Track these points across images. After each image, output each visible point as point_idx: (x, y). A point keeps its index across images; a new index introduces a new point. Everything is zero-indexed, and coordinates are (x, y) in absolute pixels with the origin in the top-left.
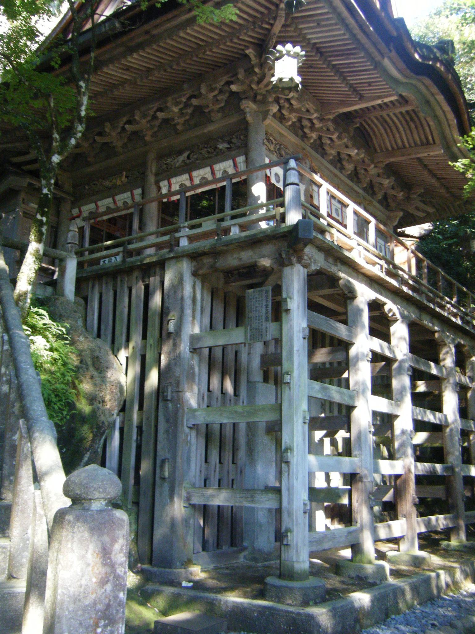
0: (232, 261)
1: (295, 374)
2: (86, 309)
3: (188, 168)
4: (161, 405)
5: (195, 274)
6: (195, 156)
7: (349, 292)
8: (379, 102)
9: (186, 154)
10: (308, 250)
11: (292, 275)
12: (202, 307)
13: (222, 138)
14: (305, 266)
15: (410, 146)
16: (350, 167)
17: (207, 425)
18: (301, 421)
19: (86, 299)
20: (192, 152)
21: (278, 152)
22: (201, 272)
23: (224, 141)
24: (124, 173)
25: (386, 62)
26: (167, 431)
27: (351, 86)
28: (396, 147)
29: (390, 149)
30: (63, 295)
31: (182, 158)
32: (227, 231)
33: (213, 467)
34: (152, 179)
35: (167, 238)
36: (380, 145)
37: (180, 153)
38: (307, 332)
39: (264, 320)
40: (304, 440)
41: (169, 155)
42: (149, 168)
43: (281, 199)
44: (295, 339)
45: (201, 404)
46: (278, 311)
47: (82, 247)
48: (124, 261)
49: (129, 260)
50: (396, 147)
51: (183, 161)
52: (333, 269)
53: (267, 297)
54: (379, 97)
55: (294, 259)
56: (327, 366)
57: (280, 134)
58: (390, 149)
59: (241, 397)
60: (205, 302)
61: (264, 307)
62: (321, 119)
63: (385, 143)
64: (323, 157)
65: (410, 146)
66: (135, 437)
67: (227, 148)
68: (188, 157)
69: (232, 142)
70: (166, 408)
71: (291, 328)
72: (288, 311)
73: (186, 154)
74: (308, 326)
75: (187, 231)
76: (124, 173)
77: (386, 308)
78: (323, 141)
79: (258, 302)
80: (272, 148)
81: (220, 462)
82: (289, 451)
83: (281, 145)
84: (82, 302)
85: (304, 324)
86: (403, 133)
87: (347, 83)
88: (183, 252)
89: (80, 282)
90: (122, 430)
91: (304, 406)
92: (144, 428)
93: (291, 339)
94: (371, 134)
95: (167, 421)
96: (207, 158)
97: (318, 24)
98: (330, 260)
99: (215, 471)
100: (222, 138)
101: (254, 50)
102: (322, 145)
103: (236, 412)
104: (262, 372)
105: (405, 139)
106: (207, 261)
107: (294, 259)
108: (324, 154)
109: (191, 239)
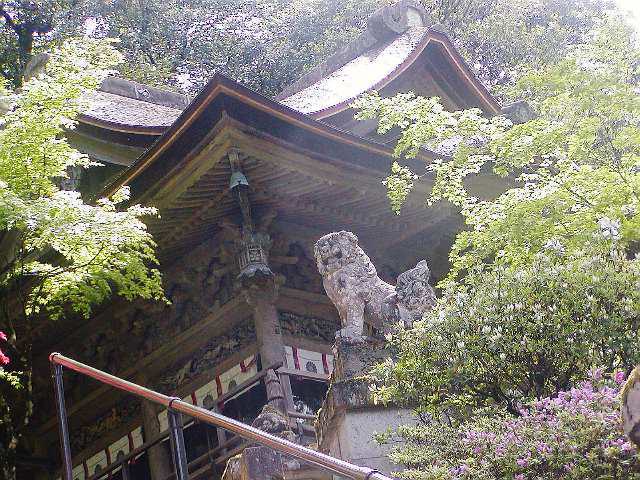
9: (188, 366)
31: (183, 372)
37: (180, 365)
51: (186, 376)
68: (192, 370)
73: (188, 366)
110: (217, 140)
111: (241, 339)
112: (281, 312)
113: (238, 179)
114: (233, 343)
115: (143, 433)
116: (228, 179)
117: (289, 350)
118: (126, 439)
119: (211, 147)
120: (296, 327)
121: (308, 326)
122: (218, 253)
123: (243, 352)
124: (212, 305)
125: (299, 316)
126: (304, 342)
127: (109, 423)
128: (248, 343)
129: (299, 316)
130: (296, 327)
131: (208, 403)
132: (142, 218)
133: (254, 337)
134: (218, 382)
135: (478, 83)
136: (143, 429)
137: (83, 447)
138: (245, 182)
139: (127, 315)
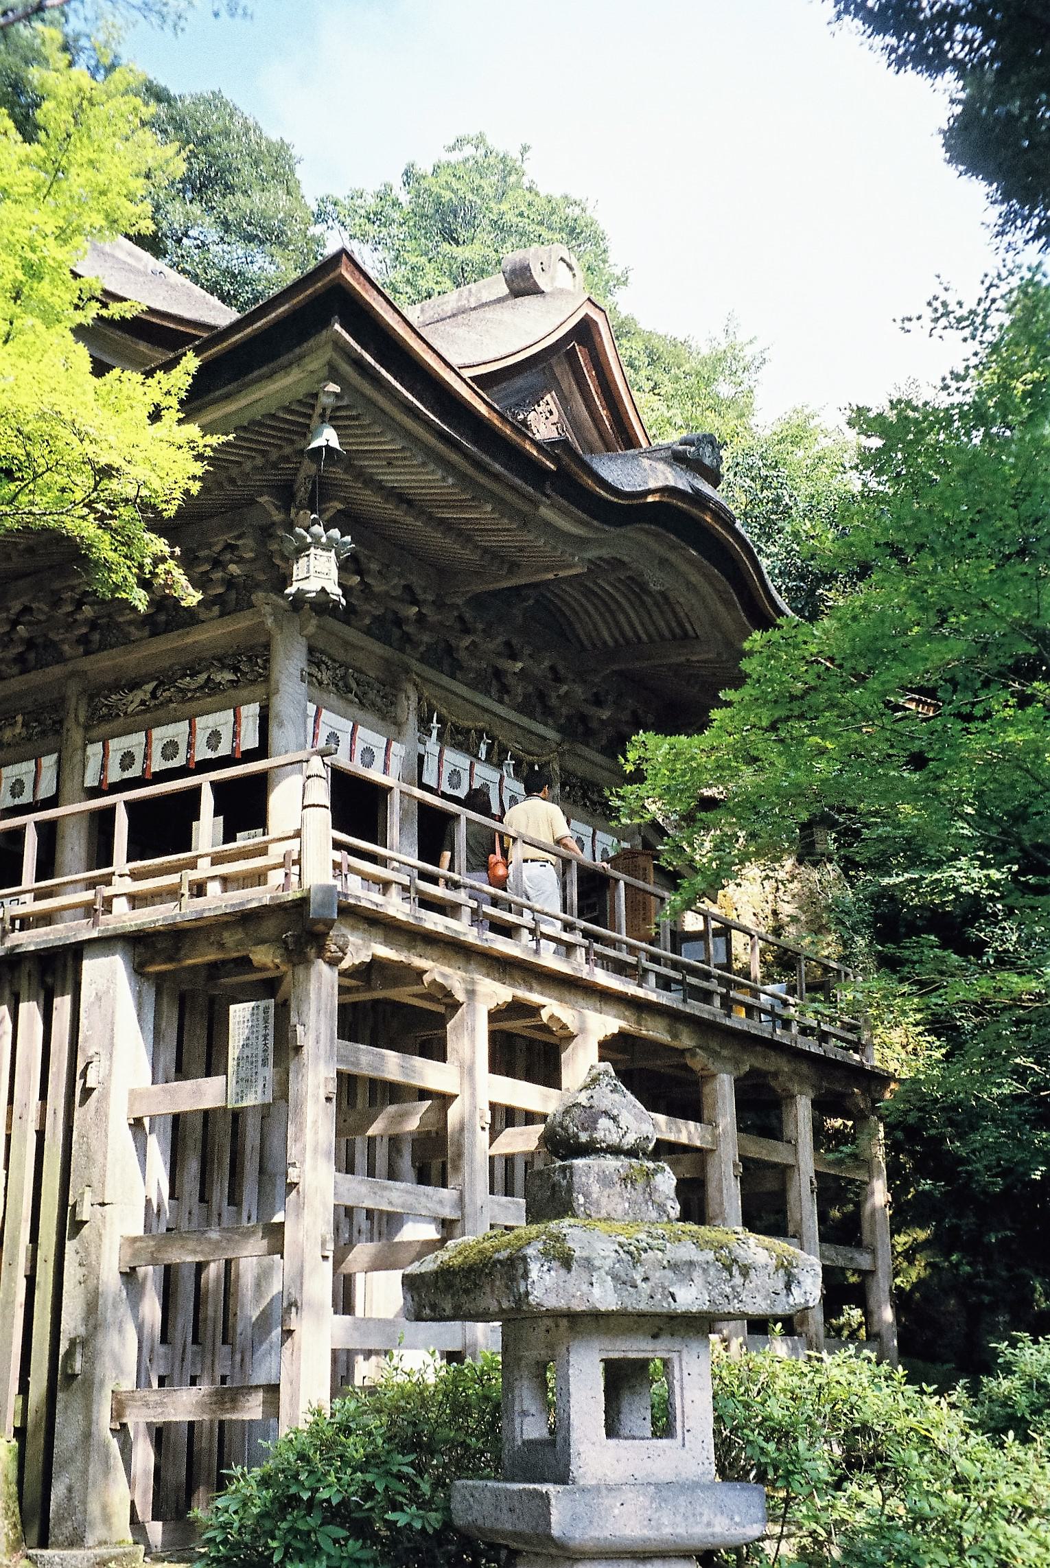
3: (149, 718)
6: (167, 694)
7: (445, 996)
8: (551, 576)
9: (149, 687)
11: (308, 980)
13: (222, 661)
14: (333, 962)
15: (651, 640)
20: (161, 683)
21: (340, 684)
23: (224, 667)
24: (19, 718)
25: (545, 512)
27: (486, 550)
29: (610, 642)
33: (179, 1351)
34: (77, 736)
36: (589, 637)
37: (134, 685)
38: (332, 1087)
39: (260, 1063)
41: (116, 687)
42: (72, 712)
45: (154, 1224)
51: (143, 703)
54: (547, 569)
55: (312, 952)
56: (434, 1135)
57: (347, 644)
58: (610, 642)
59: (245, 1206)
61: (261, 1038)
62: (439, 605)
63: (599, 633)
65: (651, 640)
67: (232, 681)
68: (154, 695)
69: (240, 670)
72: (298, 1049)
73: (149, 687)
76: (19, 718)
77: (545, 1015)
81: (195, 1341)
82: (294, 1310)
83: (347, 668)
86: (632, 615)
87: (477, 547)
97: (389, 464)
99: (183, 1360)
100: (222, 661)
101: (271, 495)
102: (450, 650)
107: (312, 952)
111: (244, 674)
112: (311, 650)
113: (769, 958)
115: (59, 762)
116: (306, 432)
117: (312, 708)
118: (32, 764)
121: (343, 678)
123: (244, 693)
125: (334, 661)
126: (333, 699)
129: (334, 661)
130: (325, 676)
131: (199, 337)
133: (267, 679)
136: (59, 759)
138: (335, 443)
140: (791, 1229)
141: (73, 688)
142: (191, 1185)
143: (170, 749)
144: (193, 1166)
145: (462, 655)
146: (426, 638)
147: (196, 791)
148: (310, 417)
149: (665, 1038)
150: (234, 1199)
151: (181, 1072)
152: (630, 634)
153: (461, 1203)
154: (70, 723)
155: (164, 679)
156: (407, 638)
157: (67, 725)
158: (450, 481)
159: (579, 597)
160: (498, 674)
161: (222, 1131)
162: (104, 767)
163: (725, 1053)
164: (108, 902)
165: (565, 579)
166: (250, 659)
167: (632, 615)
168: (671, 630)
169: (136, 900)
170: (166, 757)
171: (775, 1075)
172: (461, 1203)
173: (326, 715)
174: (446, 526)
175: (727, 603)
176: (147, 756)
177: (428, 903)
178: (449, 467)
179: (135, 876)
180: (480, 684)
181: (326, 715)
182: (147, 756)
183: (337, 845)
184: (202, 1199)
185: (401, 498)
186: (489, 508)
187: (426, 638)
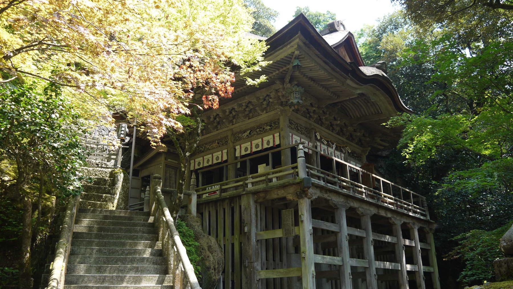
0: (274, 195)
1: (307, 253)
2: (202, 219)
4: (243, 270)
5: (256, 202)
8: (348, 98)
9: (248, 132)
10: (311, 191)
12: (261, 218)
14: (309, 198)
16: (338, 129)
17: (267, 279)
18: (311, 276)
19: (202, 214)
22: (259, 201)
26: (247, 283)
28: (362, 116)
30: (191, 213)
31: (246, 134)
32: (271, 180)
35: (241, 183)
38: (312, 231)
40: (313, 286)
43: (296, 164)
44: (306, 235)
46: (297, 221)
47: (197, 187)
48: (220, 195)
49: (223, 194)
50: (362, 116)
51: (247, 136)
52: (326, 196)
53: (292, 214)
55: (304, 196)
60: (262, 215)
64: (322, 126)
66: (230, 286)
68: (250, 133)
70: (245, 271)
71: (303, 230)
74: (313, 228)
75: (250, 180)
78: (321, 117)
79: (288, 216)
80: (293, 127)
84: (200, 215)
85: (311, 228)
88: (250, 191)
89: (199, 205)
90: (224, 282)
91: (313, 268)
92: (235, 281)
93: (304, 236)
94: (348, 109)
95: (247, 278)
96: (260, 134)
98: (323, 192)
102: (320, 119)
103: (280, 272)
104: (294, 248)
105: (366, 111)
106: (262, 195)
107: (304, 196)
108: (322, 124)
109: (253, 183)
110: (292, 44)
114: (269, 127)
117: (291, 134)
118: (249, 143)
119: (289, 46)
120: (293, 127)
122: (270, 93)
124: (263, 112)
126: (295, 132)
127: (214, 145)
128: (275, 129)
132: (113, 176)
134: (222, 152)
135: (362, 61)
137: (203, 152)
139: (245, 102)
140: (415, 262)
141: (229, 134)
142: (271, 257)
143: (257, 146)
144: (271, 252)
145: (324, 121)
146: (316, 116)
147: (268, 155)
148: (291, 58)
149: (384, 215)
150: (281, 260)
151: (267, 228)
152: (364, 113)
153: (343, 260)
154: (229, 142)
155: (252, 130)
156: (311, 117)
157: (229, 142)
158: (326, 74)
159: (351, 105)
160: (332, 125)
161: (277, 242)
162: (240, 151)
163: (398, 218)
164: (247, 184)
165: (352, 99)
166: (274, 123)
167: (365, 109)
168: (375, 112)
169: (253, 183)
170: (256, 148)
171: (409, 223)
172: (343, 260)
173: (294, 136)
174: (323, 86)
175: (390, 104)
176: (251, 148)
177: (329, 182)
178: (326, 70)
179: (253, 178)
180: (328, 128)
181: (294, 136)
182: (251, 148)
183: (308, 167)
184: (274, 260)
185: (312, 79)
186: (335, 80)
187: (316, 116)
